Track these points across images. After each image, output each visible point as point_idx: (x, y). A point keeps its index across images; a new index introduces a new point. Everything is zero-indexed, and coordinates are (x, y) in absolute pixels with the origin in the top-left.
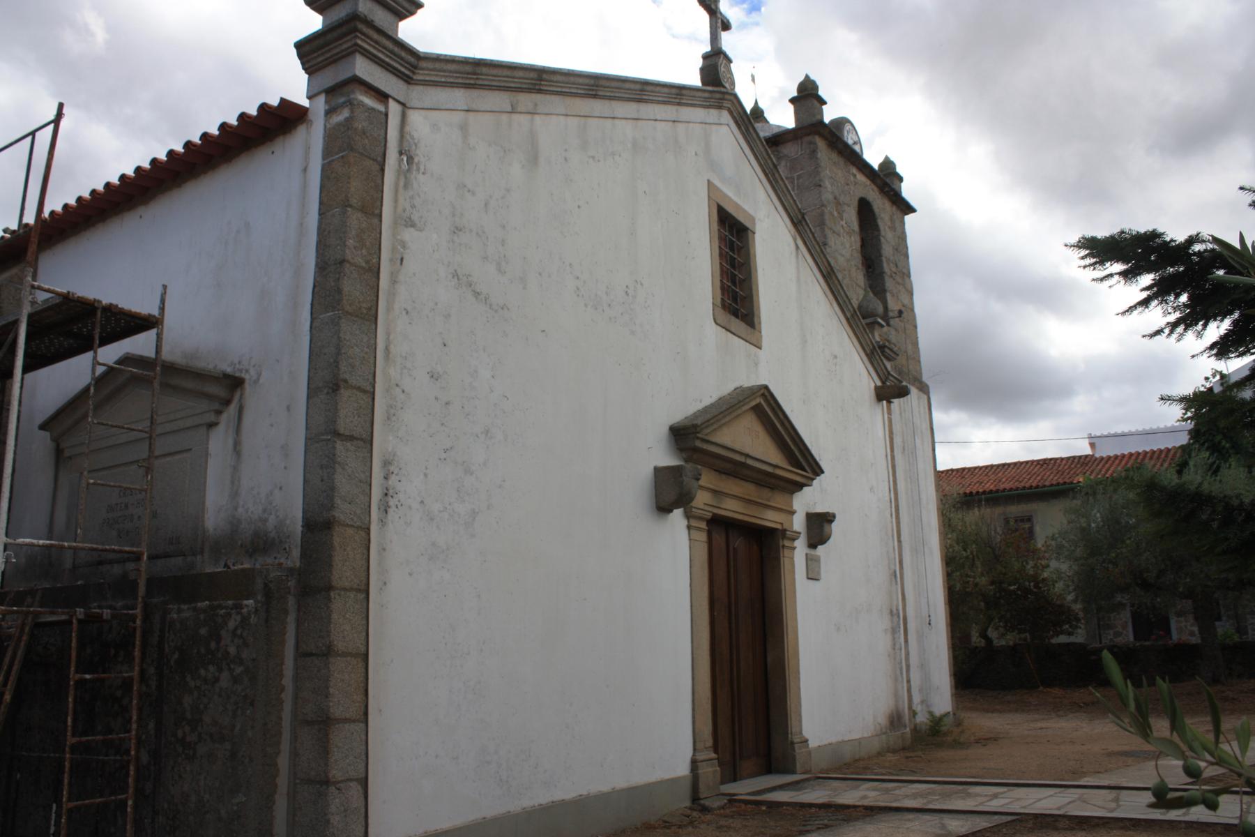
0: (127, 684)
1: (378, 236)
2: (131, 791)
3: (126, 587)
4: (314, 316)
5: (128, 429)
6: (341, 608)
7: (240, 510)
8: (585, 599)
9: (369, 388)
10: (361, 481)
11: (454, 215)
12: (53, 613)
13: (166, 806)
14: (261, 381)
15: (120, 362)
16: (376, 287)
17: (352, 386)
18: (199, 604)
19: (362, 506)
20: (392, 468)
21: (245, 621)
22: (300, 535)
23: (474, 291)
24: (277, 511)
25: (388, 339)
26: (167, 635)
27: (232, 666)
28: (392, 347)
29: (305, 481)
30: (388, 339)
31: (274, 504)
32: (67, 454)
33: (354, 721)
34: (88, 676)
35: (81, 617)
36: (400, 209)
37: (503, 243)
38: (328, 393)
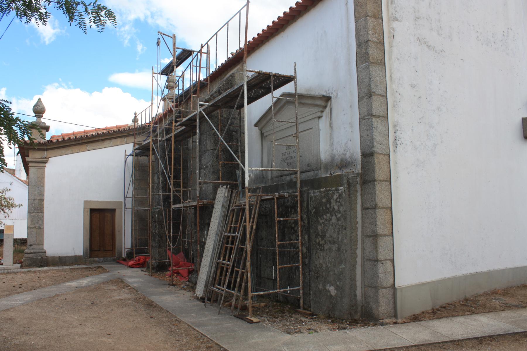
0: (296, 222)
1: (382, 27)
2: (300, 262)
3: (292, 184)
4: (358, 66)
5: (287, 122)
6: (380, 189)
7: (335, 151)
8: (489, 182)
9: (384, 94)
10: (384, 135)
11: (415, 12)
12: (267, 195)
13: (314, 268)
14: (338, 97)
15: (282, 96)
16: (383, 50)
17: (377, 94)
18: (321, 190)
19: (386, 145)
20: (397, 128)
21: (340, 195)
23: (428, 45)
24: (350, 150)
25: (391, 72)
26: (310, 202)
27: (336, 214)
28: (393, 76)
29: (361, 136)
30: (391, 72)
31: (348, 147)
32: (265, 134)
33: (388, 236)
34: (282, 219)
35: (277, 196)
36: (390, 14)
37: (439, 21)
38: (367, 98)
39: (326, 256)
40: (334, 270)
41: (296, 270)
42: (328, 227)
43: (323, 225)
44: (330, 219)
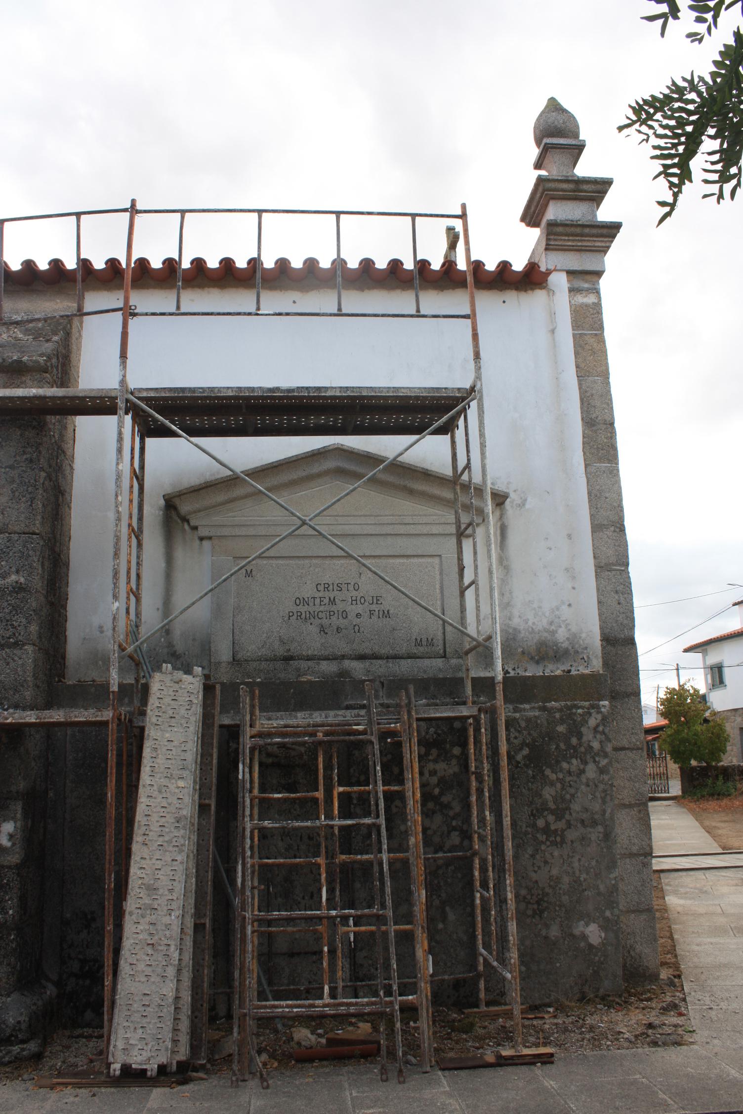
22: (600, 648)
27: (597, 759)
38: (614, 531)
39: (572, 857)
40: (598, 886)
41: (447, 909)
42: (577, 789)
43: (559, 785)
44: (579, 770)
